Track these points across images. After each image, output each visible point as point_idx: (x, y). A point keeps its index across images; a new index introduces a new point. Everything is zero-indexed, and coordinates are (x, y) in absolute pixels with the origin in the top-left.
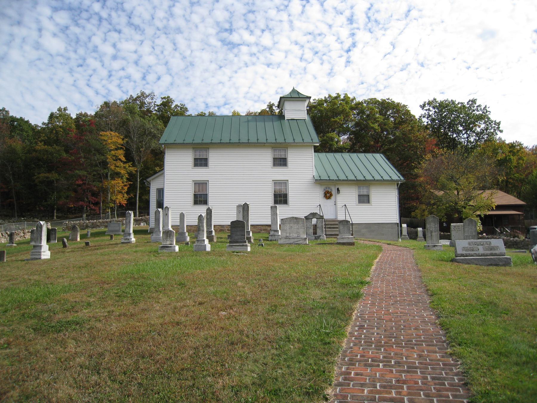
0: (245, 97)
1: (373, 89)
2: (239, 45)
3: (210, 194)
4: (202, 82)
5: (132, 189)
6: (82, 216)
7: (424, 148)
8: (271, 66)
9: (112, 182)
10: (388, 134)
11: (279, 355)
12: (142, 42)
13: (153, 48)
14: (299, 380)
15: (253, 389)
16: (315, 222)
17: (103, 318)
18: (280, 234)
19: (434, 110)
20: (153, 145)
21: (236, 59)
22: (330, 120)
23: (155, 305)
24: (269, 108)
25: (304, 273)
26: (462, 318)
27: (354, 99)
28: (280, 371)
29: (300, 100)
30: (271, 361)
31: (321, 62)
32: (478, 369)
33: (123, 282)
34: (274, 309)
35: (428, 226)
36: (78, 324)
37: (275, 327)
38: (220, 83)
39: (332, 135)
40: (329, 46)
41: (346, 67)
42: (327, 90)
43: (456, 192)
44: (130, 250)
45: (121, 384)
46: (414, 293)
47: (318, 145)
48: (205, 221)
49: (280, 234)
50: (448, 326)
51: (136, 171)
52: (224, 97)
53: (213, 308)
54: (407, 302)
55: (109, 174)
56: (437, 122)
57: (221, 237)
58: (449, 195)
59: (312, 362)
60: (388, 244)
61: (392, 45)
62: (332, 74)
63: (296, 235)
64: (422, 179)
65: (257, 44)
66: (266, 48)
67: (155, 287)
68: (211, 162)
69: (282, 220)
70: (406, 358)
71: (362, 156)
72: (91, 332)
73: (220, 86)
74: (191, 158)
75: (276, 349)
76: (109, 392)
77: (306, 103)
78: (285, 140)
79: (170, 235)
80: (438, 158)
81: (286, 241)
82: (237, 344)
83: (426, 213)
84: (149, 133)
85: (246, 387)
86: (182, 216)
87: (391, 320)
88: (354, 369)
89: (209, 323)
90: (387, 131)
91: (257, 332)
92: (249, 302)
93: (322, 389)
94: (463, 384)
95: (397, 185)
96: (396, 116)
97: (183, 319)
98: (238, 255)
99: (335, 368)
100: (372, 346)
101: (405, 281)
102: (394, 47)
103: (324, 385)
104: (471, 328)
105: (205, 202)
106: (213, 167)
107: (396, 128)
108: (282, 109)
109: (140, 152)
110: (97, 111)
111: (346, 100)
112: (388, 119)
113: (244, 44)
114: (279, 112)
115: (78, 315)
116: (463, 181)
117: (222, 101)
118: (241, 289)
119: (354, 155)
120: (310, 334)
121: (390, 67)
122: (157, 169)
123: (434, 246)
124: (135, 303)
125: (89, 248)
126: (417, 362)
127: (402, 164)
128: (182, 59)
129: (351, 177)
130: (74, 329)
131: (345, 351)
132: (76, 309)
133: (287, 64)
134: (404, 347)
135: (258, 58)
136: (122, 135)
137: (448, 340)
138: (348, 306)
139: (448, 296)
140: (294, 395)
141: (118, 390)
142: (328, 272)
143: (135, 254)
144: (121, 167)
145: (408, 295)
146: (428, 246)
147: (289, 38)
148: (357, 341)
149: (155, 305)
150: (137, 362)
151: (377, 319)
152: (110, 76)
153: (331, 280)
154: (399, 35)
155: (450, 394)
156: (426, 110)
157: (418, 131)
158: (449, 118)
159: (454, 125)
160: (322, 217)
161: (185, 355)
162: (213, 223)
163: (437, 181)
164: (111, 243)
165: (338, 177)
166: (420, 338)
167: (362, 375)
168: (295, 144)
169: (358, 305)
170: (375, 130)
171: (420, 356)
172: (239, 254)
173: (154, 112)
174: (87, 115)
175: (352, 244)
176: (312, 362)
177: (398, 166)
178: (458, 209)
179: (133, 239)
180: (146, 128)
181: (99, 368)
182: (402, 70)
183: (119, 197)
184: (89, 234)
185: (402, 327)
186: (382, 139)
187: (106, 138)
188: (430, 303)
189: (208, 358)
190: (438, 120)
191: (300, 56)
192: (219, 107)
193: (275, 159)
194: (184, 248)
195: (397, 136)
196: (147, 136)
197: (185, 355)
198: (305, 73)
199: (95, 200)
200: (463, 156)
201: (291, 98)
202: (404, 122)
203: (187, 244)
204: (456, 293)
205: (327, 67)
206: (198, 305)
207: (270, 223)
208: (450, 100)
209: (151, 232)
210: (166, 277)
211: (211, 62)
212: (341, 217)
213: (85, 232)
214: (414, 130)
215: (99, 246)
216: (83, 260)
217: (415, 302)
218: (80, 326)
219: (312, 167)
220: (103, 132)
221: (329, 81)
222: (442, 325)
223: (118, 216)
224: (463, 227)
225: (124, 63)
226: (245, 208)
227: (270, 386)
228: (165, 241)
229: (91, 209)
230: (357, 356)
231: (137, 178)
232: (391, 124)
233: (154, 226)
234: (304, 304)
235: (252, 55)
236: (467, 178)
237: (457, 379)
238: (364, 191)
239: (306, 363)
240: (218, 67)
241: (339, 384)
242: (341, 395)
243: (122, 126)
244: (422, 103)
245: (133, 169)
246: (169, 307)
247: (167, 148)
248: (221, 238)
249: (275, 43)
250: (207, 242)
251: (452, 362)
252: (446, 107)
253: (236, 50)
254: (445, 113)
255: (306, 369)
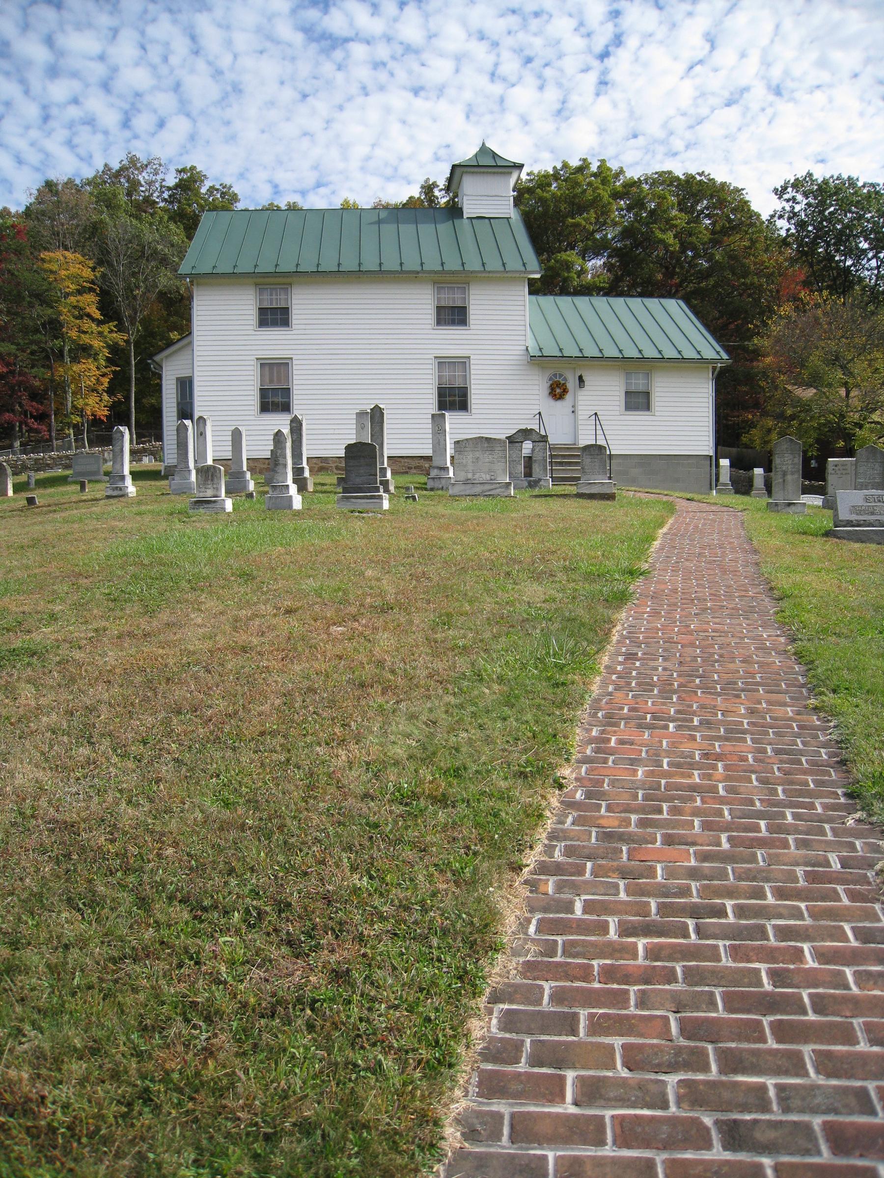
0: (363, 169)
1: (661, 149)
2: (347, 40)
3: (295, 387)
4: (263, 132)
5: (118, 384)
6: (11, 446)
7: (778, 291)
8: (422, 94)
9: (74, 369)
10: (696, 256)
11: (461, 706)
12: (115, 32)
13: (143, 48)
14: (504, 750)
15: (411, 766)
16: (529, 451)
17: (85, 642)
18: (451, 474)
19: (805, 202)
20: (164, 280)
21: (340, 76)
22: (564, 223)
23: (193, 616)
24: (426, 194)
25: (507, 552)
26: (843, 642)
27: (621, 171)
28: (465, 735)
29: (497, 173)
30: (444, 716)
31: (539, 82)
32: (869, 735)
33: (119, 572)
34: (447, 620)
35: (777, 461)
36: (35, 654)
37: (450, 654)
38: (305, 134)
39: (569, 256)
40: (558, 42)
41: (598, 94)
42: (552, 152)
43: (843, 392)
44: (125, 511)
45: (139, 761)
46: (743, 593)
47: (538, 276)
48: (289, 445)
49: (451, 474)
50: (813, 657)
51: (127, 342)
52: (316, 167)
53: (315, 621)
54: (727, 612)
55: (67, 348)
56: (810, 228)
57: (322, 482)
58: (827, 398)
59: (529, 717)
60: (688, 500)
61: (707, 40)
62: (565, 114)
63: (488, 477)
64: (768, 360)
65: (389, 39)
66: (409, 49)
67: (189, 581)
68: (297, 316)
69: (457, 443)
70: (723, 715)
71: (636, 303)
72: (64, 668)
73: (305, 143)
74: (251, 307)
75: (454, 694)
76: (116, 776)
77: (512, 181)
78: (463, 264)
79: (212, 476)
80: (809, 314)
81: (465, 490)
82: (372, 687)
83: (774, 436)
84: (152, 254)
85: (396, 763)
86: (236, 436)
87: (692, 645)
88: (615, 732)
89: (311, 647)
90: (694, 249)
91: (414, 664)
92: (392, 608)
93: (553, 767)
94: (838, 762)
95: (714, 369)
96: (717, 214)
97: (255, 641)
98: (363, 518)
99: (578, 731)
100: (652, 691)
101: (724, 572)
102: (713, 47)
103: (554, 760)
104: (860, 660)
105: (286, 408)
106: (303, 327)
107: (715, 242)
108: (456, 196)
109: (135, 297)
110: (31, 204)
111: (604, 174)
112: (697, 220)
113: (356, 38)
114: (448, 202)
115: (31, 638)
116: (859, 367)
117: (310, 178)
118: (374, 583)
119: (619, 303)
120: (524, 666)
121: (700, 96)
122: (174, 335)
123: (789, 504)
124: (149, 612)
125: (36, 510)
126: (745, 721)
127: (725, 326)
128: (213, 76)
129: (611, 351)
130: (29, 664)
131: (597, 701)
132: (26, 626)
133: (460, 88)
134: (719, 695)
135: (392, 74)
136: (90, 259)
137: (810, 683)
138: (602, 615)
139: (814, 601)
140: (494, 777)
141: (134, 771)
142: (559, 552)
143: (138, 518)
144: (92, 332)
145: (729, 596)
146: (776, 504)
147: (464, 22)
148: (622, 682)
149: (193, 616)
150: (167, 722)
151: (664, 642)
152: (46, 118)
153: (564, 567)
154: (726, 15)
155: (810, 778)
156: (788, 201)
157: (766, 250)
158: (840, 221)
159: (849, 236)
160: (544, 439)
161: (266, 708)
162: (306, 452)
163: (803, 366)
164: (84, 498)
165: (581, 350)
166: (754, 678)
167: (632, 744)
168: (487, 275)
169: (623, 615)
170: (666, 246)
171: (752, 712)
172: (364, 515)
173: (162, 204)
174: (9, 213)
175: (611, 497)
176: (529, 717)
177: (718, 331)
178: (845, 429)
179: (131, 489)
180: (146, 243)
181: (90, 733)
182: (728, 105)
183: (92, 400)
184: (33, 481)
185: (716, 657)
186: (682, 268)
187: (55, 267)
188: (776, 613)
189: (314, 713)
190: (813, 225)
191: (489, 67)
192: (303, 193)
193: (439, 309)
194: (244, 504)
195: (717, 261)
196: (147, 260)
197: (266, 708)
198: (503, 110)
199: (37, 410)
200: (865, 309)
201: (479, 166)
202: (733, 228)
203: (250, 495)
204: (832, 595)
205: (552, 95)
206: (284, 614)
207: (429, 452)
208: (845, 176)
209: (168, 474)
210: (210, 562)
211: (282, 83)
212: (585, 440)
213: (23, 478)
214: (757, 248)
215: (56, 505)
216: (28, 533)
217: (745, 612)
218: (40, 657)
219: (522, 328)
220: (47, 253)
221: (558, 129)
222: (799, 656)
223: (92, 444)
224: (854, 468)
225: (75, 85)
226: (376, 416)
227: (444, 761)
228: (203, 490)
229: (30, 430)
230: (622, 709)
231: (129, 358)
232: (705, 232)
233: (175, 461)
234: (509, 611)
235: (378, 65)
236: (871, 360)
237: (826, 754)
238: (638, 384)
239: (517, 720)
240: (298, 97)
241: (585, 760)
242: (590, 779)
243: (90, 238)
244: (779, 184)
245: (119, 338)
246: (223, 618)
247: (198, 284)
248: (323, 485)
249: (431, 36)
250: (293, 489)
251: (818, 723)
252: (836, 194)
253: (338, 54)
254: (832, 209)
255: (518, 730)
